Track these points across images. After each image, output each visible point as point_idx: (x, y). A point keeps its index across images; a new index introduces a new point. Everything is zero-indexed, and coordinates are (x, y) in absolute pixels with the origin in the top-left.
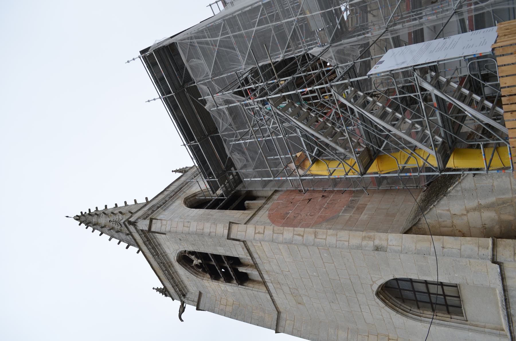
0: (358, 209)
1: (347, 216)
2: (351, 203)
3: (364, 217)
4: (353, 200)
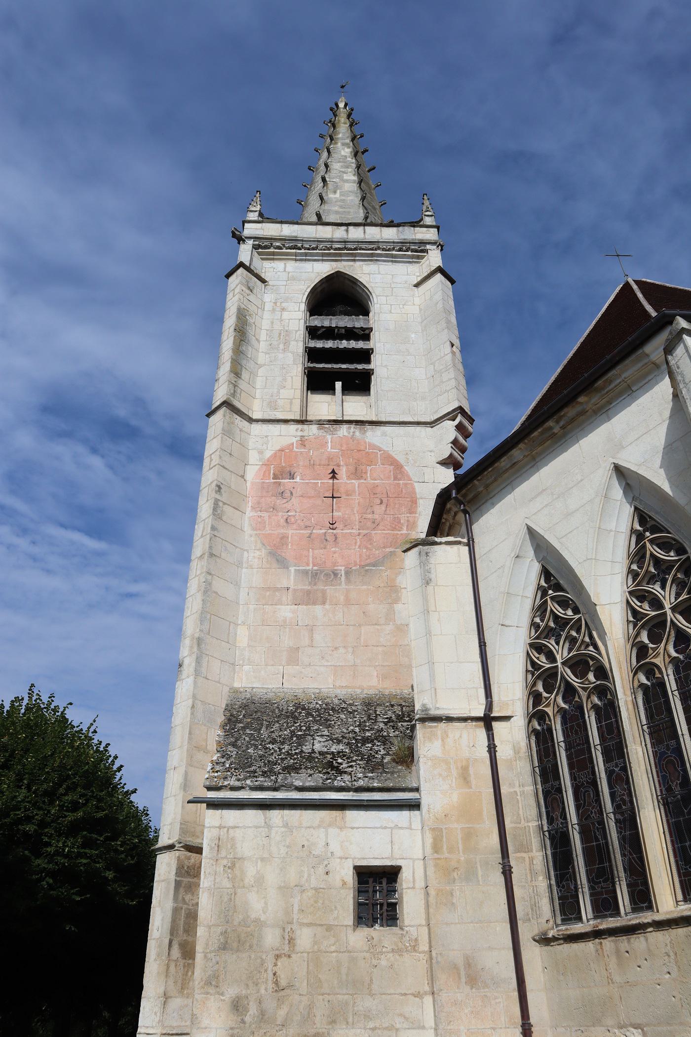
0: (308, 593)
1: (289, 579)
2: (327, 575)
3: (286, 611)
4: (336, 575)
